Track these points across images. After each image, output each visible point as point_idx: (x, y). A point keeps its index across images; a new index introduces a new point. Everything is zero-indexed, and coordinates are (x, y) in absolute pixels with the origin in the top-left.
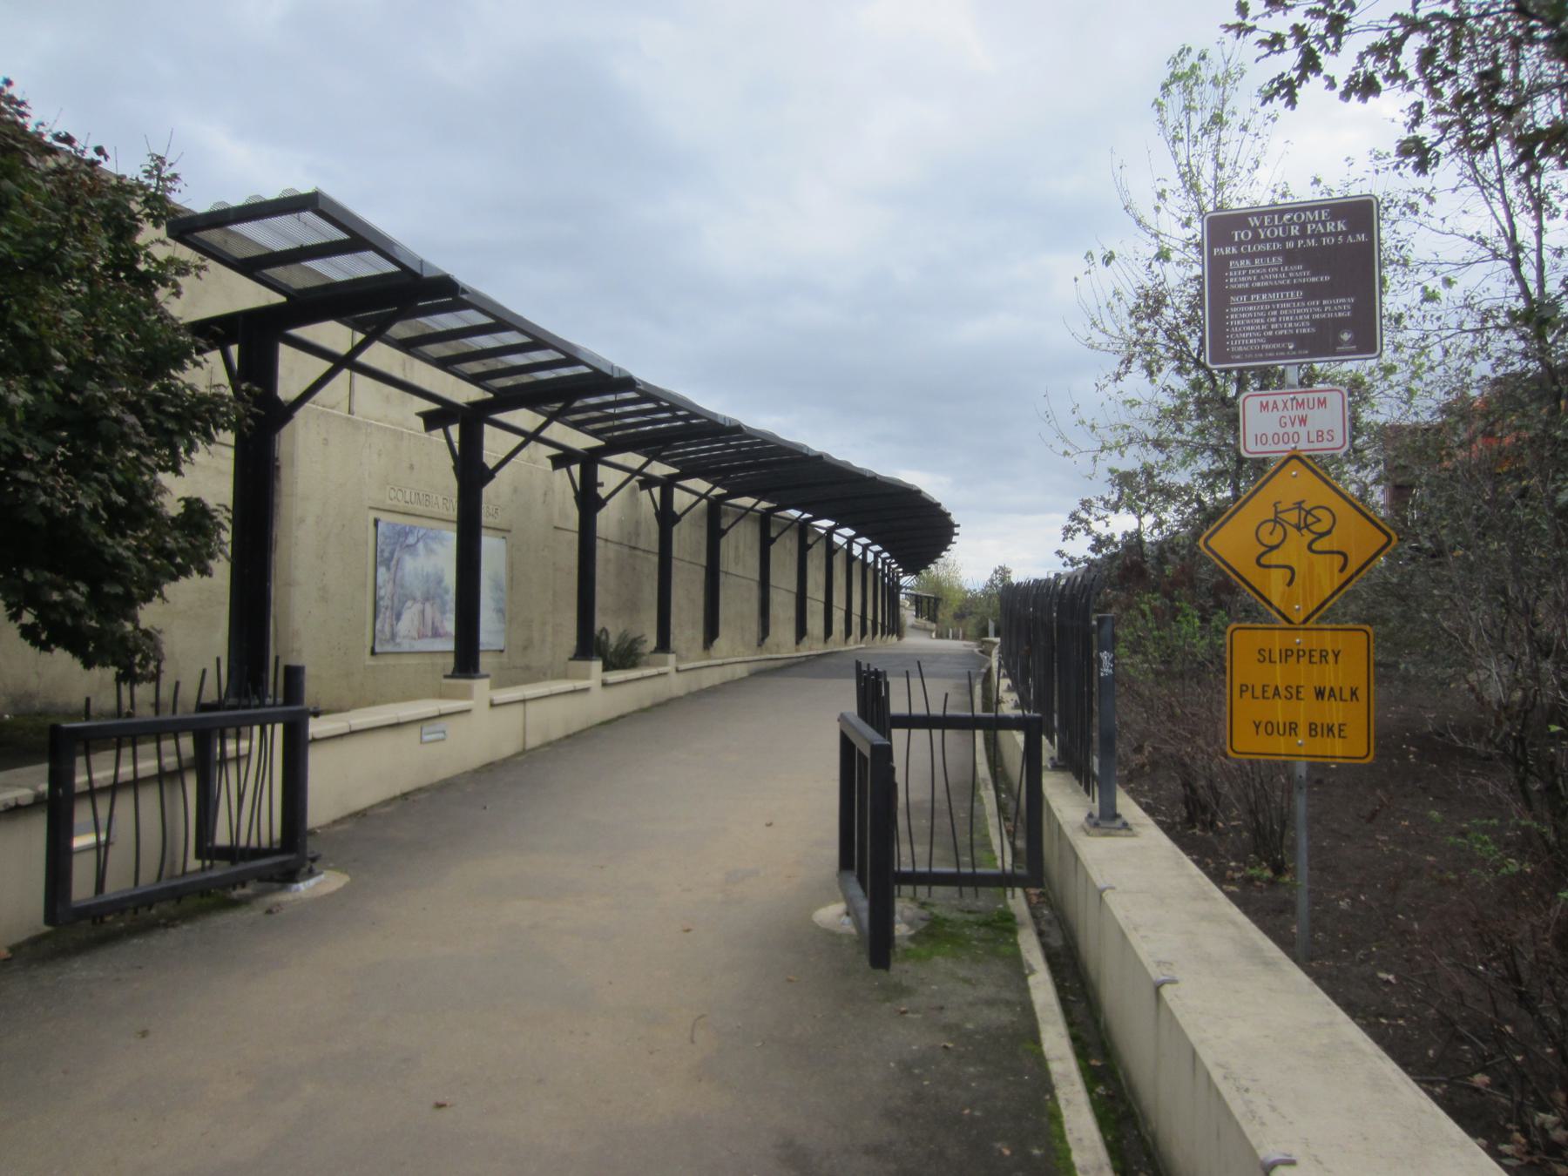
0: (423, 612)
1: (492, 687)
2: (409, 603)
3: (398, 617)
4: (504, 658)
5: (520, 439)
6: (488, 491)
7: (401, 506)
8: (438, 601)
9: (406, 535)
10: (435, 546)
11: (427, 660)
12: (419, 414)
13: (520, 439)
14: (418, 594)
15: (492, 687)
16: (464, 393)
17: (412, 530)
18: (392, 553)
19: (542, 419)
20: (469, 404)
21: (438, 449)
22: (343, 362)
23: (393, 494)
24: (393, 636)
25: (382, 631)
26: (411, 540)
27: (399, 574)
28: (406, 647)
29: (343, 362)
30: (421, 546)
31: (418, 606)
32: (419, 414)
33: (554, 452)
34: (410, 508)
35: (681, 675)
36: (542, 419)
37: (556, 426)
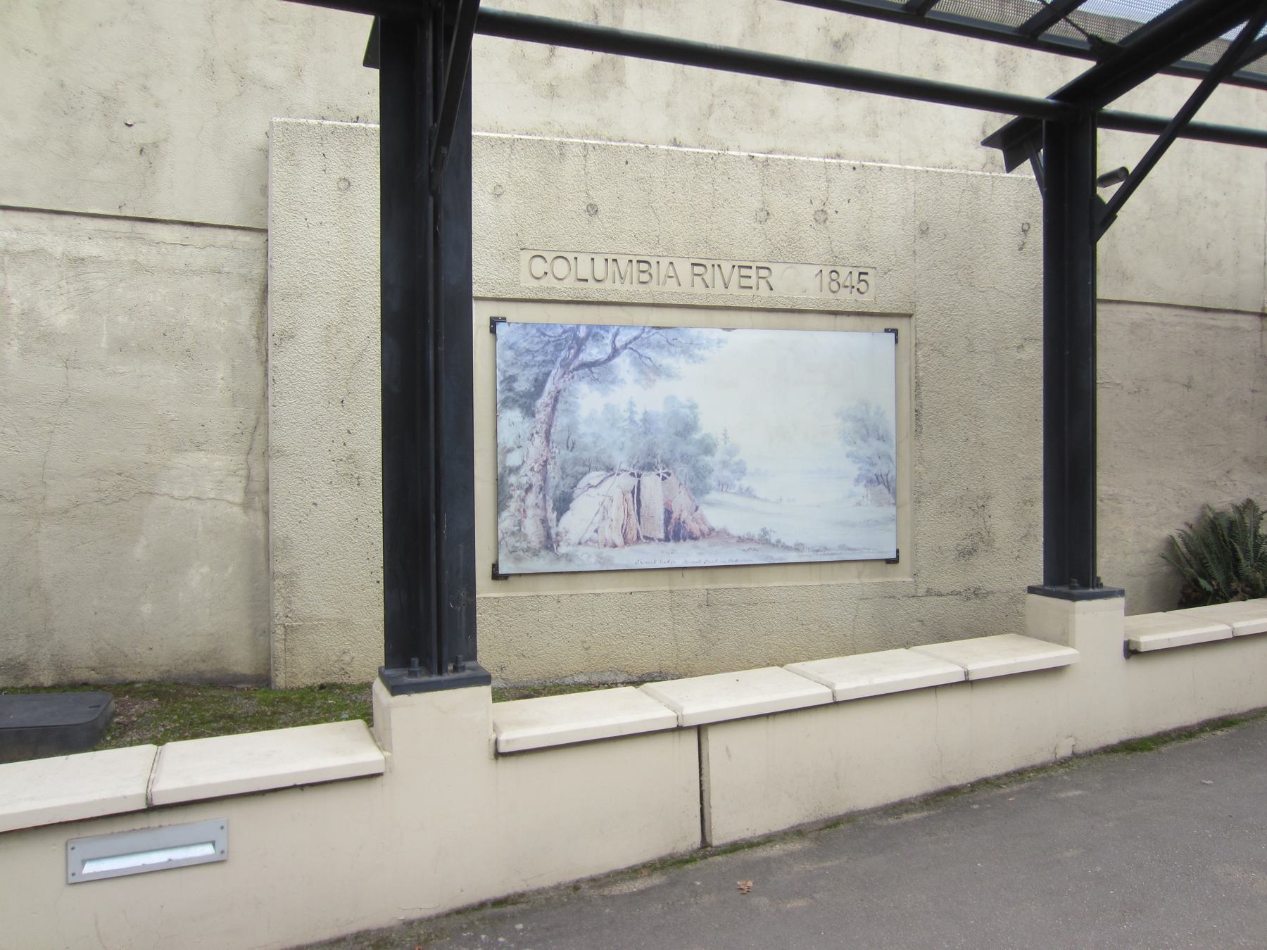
0: (637, 492)
1: (1130, 611)
2: (593, 477)
3: (563, 504)
4: (900, 576)
5: (1151, 139)
6: (1111, 248)
7: (568, 288)
8: (682, 469)
9: (580, 344)
10: (665, 360)
11: (660, 585)
12: (989, 142)
13: (1151, 139)
14: (620, 460)
15: (1130, 611)
16: (1042, 76)
17: (594, 334)
18: (539, 385)
19: (1191, 85)
20: (1054, 96)
21: (1020, 192)
22: (1182, 126)
23: (539, 267)
24: (549, 542)
25: (518, 532)
26: (593, 352)
27: (561, 421)
28: (588, 559)
29: (1182, 126)
30: (623, 363)
31: (627, 482)
32: (989, 142)
33: (998, 121)
34: (592, 291)
35: (1138, 669)
36: (1191, 85)
37: (1223, 91)
